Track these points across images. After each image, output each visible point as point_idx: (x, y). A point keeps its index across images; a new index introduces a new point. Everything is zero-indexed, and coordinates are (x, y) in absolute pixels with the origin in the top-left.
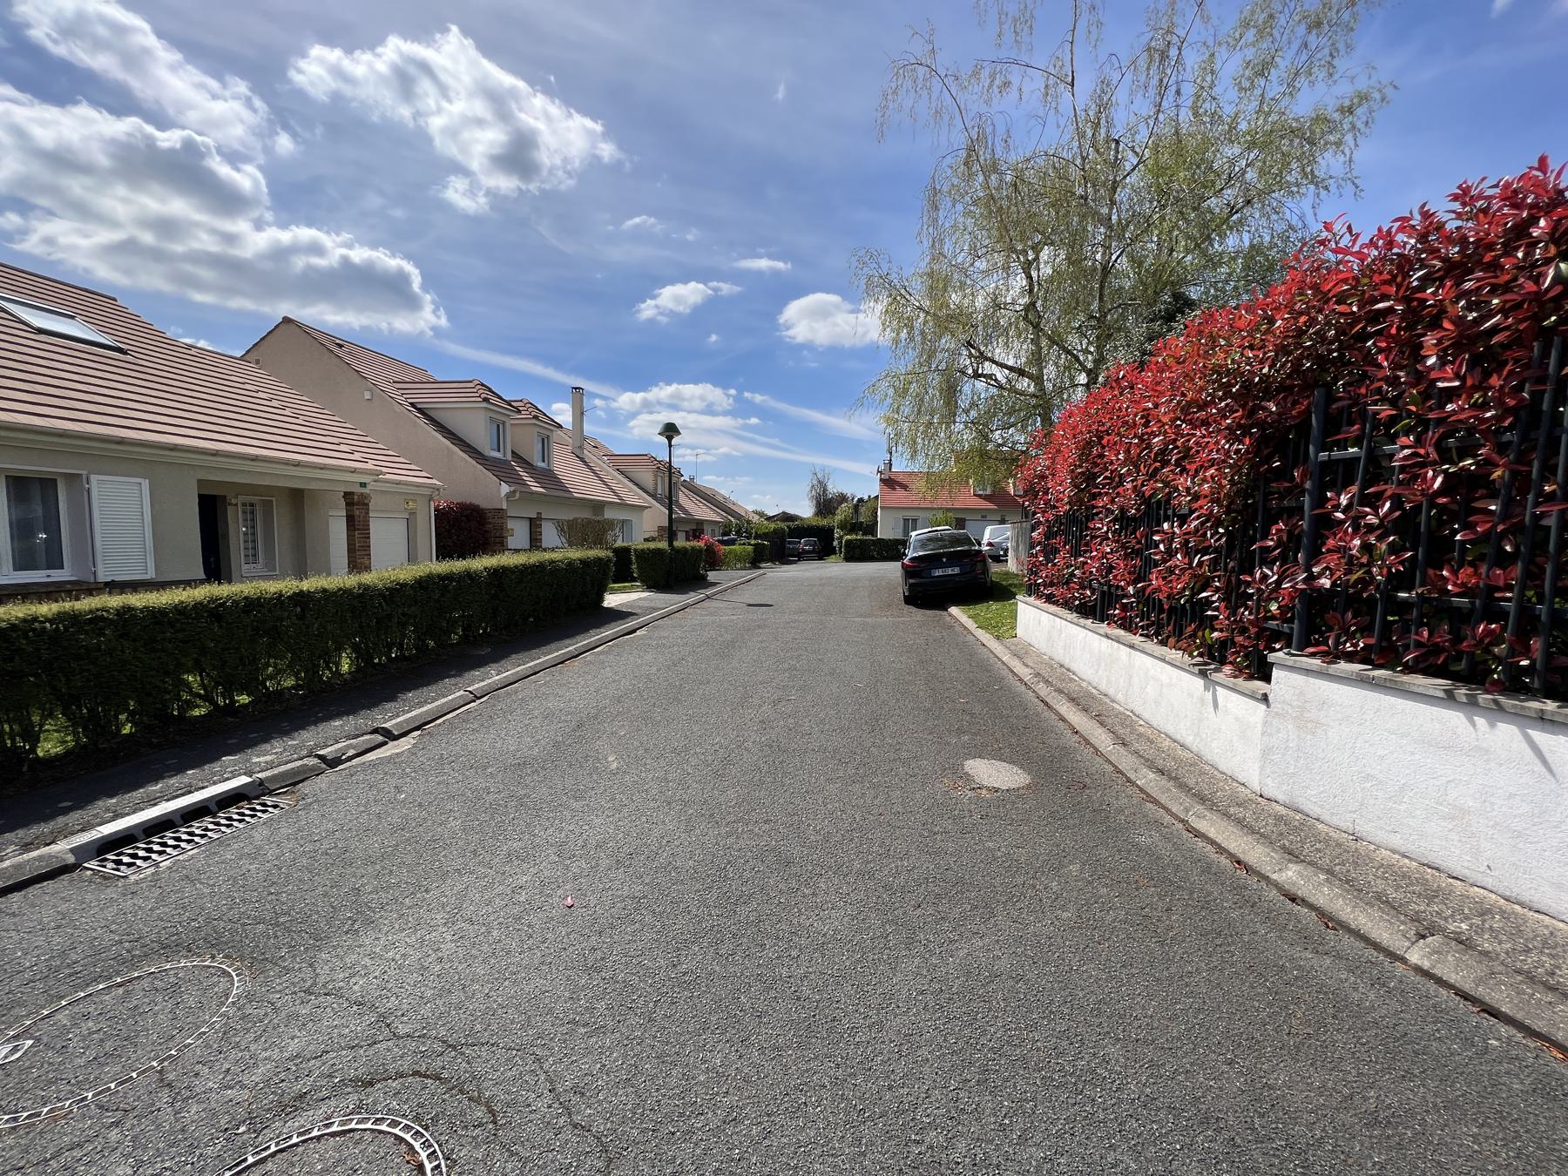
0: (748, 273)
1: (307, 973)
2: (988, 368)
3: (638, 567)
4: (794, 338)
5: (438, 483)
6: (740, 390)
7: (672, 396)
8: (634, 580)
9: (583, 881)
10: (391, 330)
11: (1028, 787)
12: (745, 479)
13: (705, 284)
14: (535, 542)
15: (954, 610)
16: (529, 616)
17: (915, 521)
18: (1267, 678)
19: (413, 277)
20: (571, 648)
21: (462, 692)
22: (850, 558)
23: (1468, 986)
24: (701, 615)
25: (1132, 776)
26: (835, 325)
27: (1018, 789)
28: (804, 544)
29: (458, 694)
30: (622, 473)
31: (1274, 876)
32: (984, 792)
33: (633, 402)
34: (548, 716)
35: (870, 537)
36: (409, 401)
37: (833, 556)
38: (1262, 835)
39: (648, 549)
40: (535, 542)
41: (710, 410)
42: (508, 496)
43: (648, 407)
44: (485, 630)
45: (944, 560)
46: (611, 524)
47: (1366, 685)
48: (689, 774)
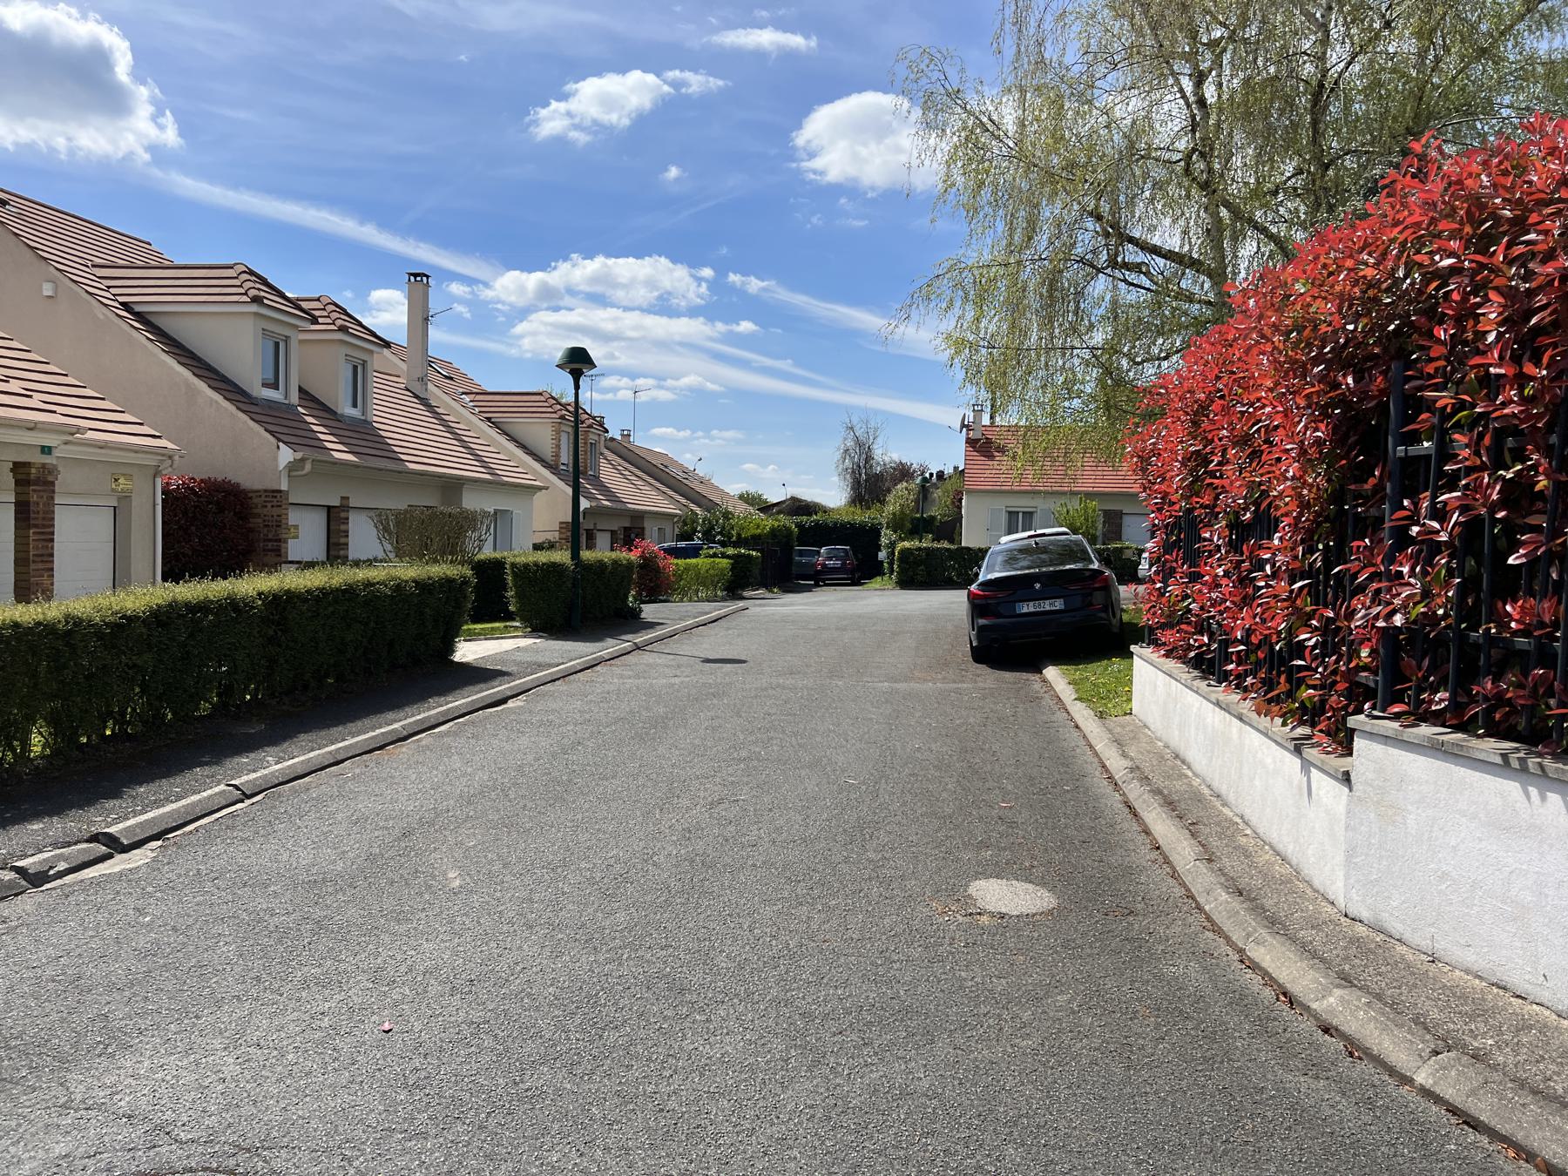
0: (740, 57)
1: (60, 1091)
2: (1132, 254)
3: (518, 595)
4: (822, 173)
5: (170, 446)
6: (721, 270)
7: (595, 279)
8: (510, 617)
9: (404, 1007)
10: (72, 152)
11: (1050, 912)
12: (729, 434)
13: (658, 76)
14: (336, 551)
15: (1051, 672)
16: (327, 676)
17: (1029, 515)
18: (1349, 752)
19: (117, 55)
20: (396, 726)
21: (222, 787)
22: (908, 582)
23: (1458, 1101)
24: (622, 676)
25: (1201, 900)
26: (898, 150)
27: (1034, 915)
28: (824, 555)
29: (217, 790)
30: (496, 425)
31: (1314, 1006)
32: (985, 919)
33: (522, 289)
34: (359, 821)
35: (946, 545)
36: (121, 299)
37: (879, 579)
38: (1323, 960)
39: (536, 564)
40: (336, 551)
41: (664, 306)
42: (292, 467)
43: (549, 298)
44: (254, 697)
45: (1038, 586)
46: (470, 520)
47: (1440, 754)
48: (564, 894)
